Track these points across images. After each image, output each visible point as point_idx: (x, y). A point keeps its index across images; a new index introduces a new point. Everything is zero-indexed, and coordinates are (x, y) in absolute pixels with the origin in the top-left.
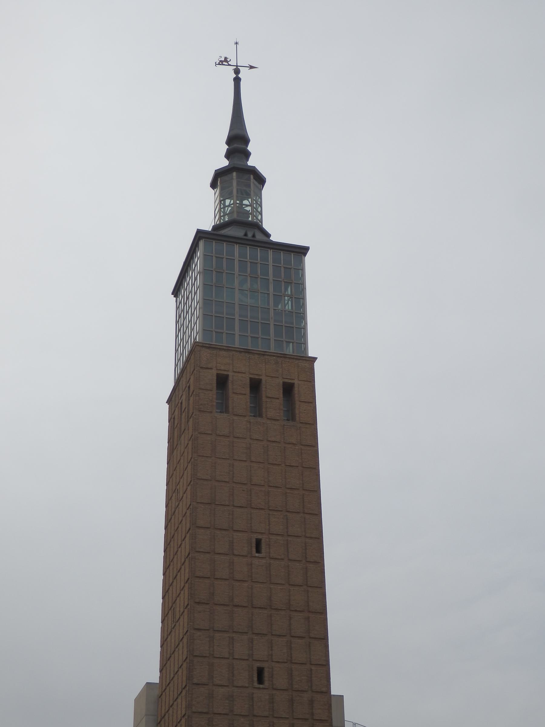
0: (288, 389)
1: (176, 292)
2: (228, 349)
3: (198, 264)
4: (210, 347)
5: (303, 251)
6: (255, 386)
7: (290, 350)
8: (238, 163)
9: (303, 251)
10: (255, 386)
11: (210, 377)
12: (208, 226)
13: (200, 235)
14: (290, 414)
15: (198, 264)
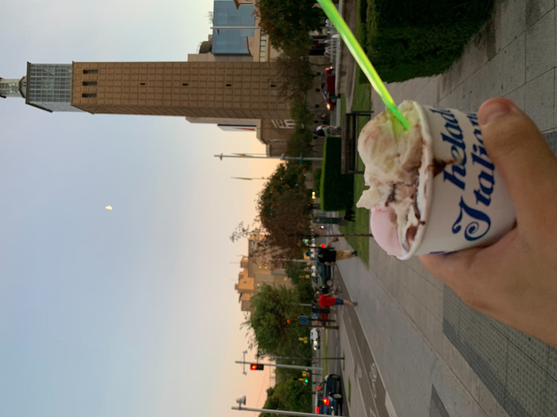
0: (85, 72)
1: (51, 111)
2: (72, 94)
5: (29, 64)
6: (85, 84)
7: (70, 71)
9: (29, 64)
10: (85, 84)
11: (84, 100)
13: (28, 103)
14: (95, 71)
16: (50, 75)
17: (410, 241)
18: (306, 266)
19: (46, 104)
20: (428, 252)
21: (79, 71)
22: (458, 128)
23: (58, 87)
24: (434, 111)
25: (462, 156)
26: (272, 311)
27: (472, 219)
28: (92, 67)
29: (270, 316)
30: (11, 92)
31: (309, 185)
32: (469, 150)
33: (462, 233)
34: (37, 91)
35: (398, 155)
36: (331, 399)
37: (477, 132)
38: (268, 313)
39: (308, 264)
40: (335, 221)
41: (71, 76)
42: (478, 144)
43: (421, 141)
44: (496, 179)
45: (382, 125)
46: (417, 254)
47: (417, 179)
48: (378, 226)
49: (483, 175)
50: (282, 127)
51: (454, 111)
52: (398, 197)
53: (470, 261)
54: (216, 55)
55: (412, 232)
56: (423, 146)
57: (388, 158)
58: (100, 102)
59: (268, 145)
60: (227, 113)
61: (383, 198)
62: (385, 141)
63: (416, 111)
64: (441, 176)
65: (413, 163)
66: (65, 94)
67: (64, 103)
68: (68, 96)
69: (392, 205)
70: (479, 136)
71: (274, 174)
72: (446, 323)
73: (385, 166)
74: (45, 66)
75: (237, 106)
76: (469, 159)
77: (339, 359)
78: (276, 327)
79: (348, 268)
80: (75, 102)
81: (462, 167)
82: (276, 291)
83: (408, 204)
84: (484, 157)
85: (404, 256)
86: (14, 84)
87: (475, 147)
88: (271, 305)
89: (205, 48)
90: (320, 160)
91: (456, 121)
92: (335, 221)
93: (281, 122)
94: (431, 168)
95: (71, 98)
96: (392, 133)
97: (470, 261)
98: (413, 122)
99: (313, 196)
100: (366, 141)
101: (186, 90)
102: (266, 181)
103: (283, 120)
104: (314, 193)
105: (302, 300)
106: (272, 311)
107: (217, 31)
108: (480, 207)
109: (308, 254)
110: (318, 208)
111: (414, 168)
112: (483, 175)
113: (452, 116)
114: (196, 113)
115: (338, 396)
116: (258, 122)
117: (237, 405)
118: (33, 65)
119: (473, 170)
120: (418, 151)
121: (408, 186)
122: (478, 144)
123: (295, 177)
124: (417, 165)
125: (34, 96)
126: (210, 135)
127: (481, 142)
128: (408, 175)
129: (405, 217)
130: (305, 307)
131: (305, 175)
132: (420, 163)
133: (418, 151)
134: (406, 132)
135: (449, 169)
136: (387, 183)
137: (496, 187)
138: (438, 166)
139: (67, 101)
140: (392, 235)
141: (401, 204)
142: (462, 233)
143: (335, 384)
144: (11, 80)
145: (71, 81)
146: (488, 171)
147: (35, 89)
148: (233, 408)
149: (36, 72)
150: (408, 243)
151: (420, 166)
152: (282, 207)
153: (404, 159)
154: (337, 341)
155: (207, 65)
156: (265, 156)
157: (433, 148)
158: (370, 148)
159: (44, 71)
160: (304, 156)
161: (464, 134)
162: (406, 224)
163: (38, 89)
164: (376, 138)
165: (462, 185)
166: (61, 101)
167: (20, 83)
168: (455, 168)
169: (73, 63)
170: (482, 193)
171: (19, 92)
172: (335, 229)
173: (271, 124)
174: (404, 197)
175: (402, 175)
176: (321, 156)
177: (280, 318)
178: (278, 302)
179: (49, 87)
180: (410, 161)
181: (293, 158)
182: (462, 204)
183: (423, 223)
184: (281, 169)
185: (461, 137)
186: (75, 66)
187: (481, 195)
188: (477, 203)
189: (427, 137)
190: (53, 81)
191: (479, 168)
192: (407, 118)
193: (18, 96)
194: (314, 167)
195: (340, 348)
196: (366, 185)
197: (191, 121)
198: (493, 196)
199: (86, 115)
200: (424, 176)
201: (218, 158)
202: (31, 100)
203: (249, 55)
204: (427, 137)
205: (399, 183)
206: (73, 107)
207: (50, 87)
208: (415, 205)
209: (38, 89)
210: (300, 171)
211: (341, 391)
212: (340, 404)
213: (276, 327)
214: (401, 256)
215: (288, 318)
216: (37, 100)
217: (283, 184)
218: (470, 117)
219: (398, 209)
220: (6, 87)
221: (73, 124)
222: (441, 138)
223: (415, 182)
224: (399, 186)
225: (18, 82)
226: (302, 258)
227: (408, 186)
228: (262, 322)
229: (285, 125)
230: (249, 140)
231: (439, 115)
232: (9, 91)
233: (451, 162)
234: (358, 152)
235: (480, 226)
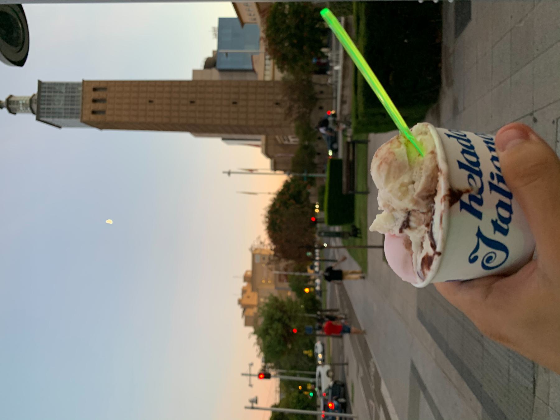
0: (95, 89)
1: (59, 127)
2: (82, 110)
3: (49, 120)
4: (82, 117)
5: (40, 83)
6: (95, 101)
7: (80, 89)
8: (5, 105)
9: (40, 83)
10: (95, 101)
11: (93, 117)
12: (34, 117)
13: (38, 119)
14: (104, 89)
15: (49, 120)
16: (61, 92)
17: (426, 271)
18: (310, 280)
19: (56, 121)
20: (444, 281)
21: (89, 89)
22: (474, 155)
23: (68, 105)
24: (449, 136)
25: (479, 185)
26: (279, 320)
27: (490, 250)
28: (102, 85)
29: (277, 326)
30: (21, 108)
31: (312, 199)
32: (486, 178)
33: (479, 262)
34: (48, 109)
35: (413, 183)
36: (335, 403)
37: (494, 159)
38: (276, 322)
39: (313, 277)
40: (338, 234)
41: (80, 94)
42: (495, 171)
43: (437, 168)
44: (514, 208)
45: (396, 150)
46: (434, 282)
47: (433, 207)
48: (393, 251)
49: (501, 204)
50: (286, 142)
51: (470, 135)
52: (412, 224)
53: (488, 291)
54: (221, 71)
55: (427, 262)
56: (439, 173)
57: (402, 185)
58: (109, 119)
59: (273, 160)
60: (232, 129)
61: (397, 224)
62: (398, 168)
63: (431, 136)
64: (457, 205)
65: (429, 191)
66: (75, 111)
67: (74, 120)
68: (77, 113)
69: (406, 231)
70: (496, 163)
71: (280, 191)
72: (419, 309)
73: (400, 194)
74: (55, 84)
75: (243, 123)
76: (487, 187)
77: (343, 364)
78: (283, 336)
79: (354, 285)
80: (85, 119)
81: (479, 197)
82: (283, 302)
83: (423, 232)
84: (501, 185)
85: (420, 284)
86: (24, 102)
87: (492, 175)
88: (278, 315)
89: (210, 64)
90: (324, 177)
91: (472, 147)
92: (338, 234)
93: (285, 138)
94: (447, 198)
95: (80, 115)
96: (406, 159)
97: (488, 291)
98: (430, 149)
99: (318, 212)
100: (379, 167)
101: (192, 108)
102: (273, 196)
103: (287, 137)
104: (317, 206)
105: (308, 310)
106: (279, 320)
107: (220, 45)
108: (498, 237)
109: (312, 267)
110: (322, 222)
111: (430, 195)
112: (501, 204)
113: (469, 141)
114: (200, 129)
115: (342, 400)
116: (263, 137)
117: (250, 405)
118: (44, 83)
119: (491, 198)
120: (433, 179)
121: (423, 213)
122: (495, 171)
123: (299, 193)
124: (432, 193)
125: (44, 113)
126: (215, 151)
127: (498, 169)
128: (423, 203)
129: (420, 244)
130: (310, 318)
131: (309, 190)
132: (436, 191)
133: (433, 179)
134: (421, 158)
135: (465, 198)
136: (402, 210)
137: (513, 216)
138: (454, 196)
139: (76, 117)
140: (407, 262)
141: (416, 231)
142: (479, 262)
143: (339, 390)
144: (21, 97)
145: (81, 98)
146: (506, 200)
147: (46, 106)
148: (246, 408)
149: (47, 90)
150: (424, 273)
151: (435, 194)
152: (288, 221)
153: (419, 186)
154: (341, 350)
155: (213, 84)
156: (270, 171)
157: (449, 178)
158: (383, 174)
159: (54, 88)
160: (309, 172)
161: (480, 161)
162: (421, 252)
163: (49, 107)
164: (390, 164)
165: (479, 215)
166: (71, 117)
167: (31, 100)
168: (472, 198)
169: (84, 81)
170: (499, 222)
171: (29, 109)
172: (338, 241)
173: (275, 140)
174: (419, 225)
175: (416, 203)
176: (324, 172)
177: (286, 327)
178: (285, 312)
179: (59, 104)
180: (424, 189)
181: (297, 174)
182: (479, 234)
183: (439, 254)
184: (287, 185)
185: (477, 164)
186: (85, 84)
187: (499, 225)
188: (495, 233)
189: (442, 166)
190: (63, 98)
191: (497, 197)
192: (421, 143)
193: (28, 112)
194: (318, 183)
195: (344, 356)
196: (379, 209)
197: (196, 136)
198: (511, 226)
199: (94, 131)
200: (440, 205)
201: (226, 175)
202: (41, 117)
203: (253, 70)
204: (442, 166)
205: (414, 210)
206: (83, 124)
207: (59, 104)
208: (431, 235)
209: (49, 107)
210: (305, 187)
211: (345, 396)
212: (344, 407)
213: (283, 336)
214: (416, 283)
215: (294, 328)
216: (47, 117)
217: (289, 200)
218: (487, 142)
219: (414, 236)
220: (17, 104)
221: (81, 139)
222: (457, 165)
223: (431, 211)
224: (413, 213)
225: (28, 99)
226: (306, 271)
227: (423, 213)
228: (270, 331)
229: (289, 140)
230: (250, 155)
231: (455, 140)
232: (19, 108)
233: (468, 191)
234: (371, 177)
235: (497, 256)
